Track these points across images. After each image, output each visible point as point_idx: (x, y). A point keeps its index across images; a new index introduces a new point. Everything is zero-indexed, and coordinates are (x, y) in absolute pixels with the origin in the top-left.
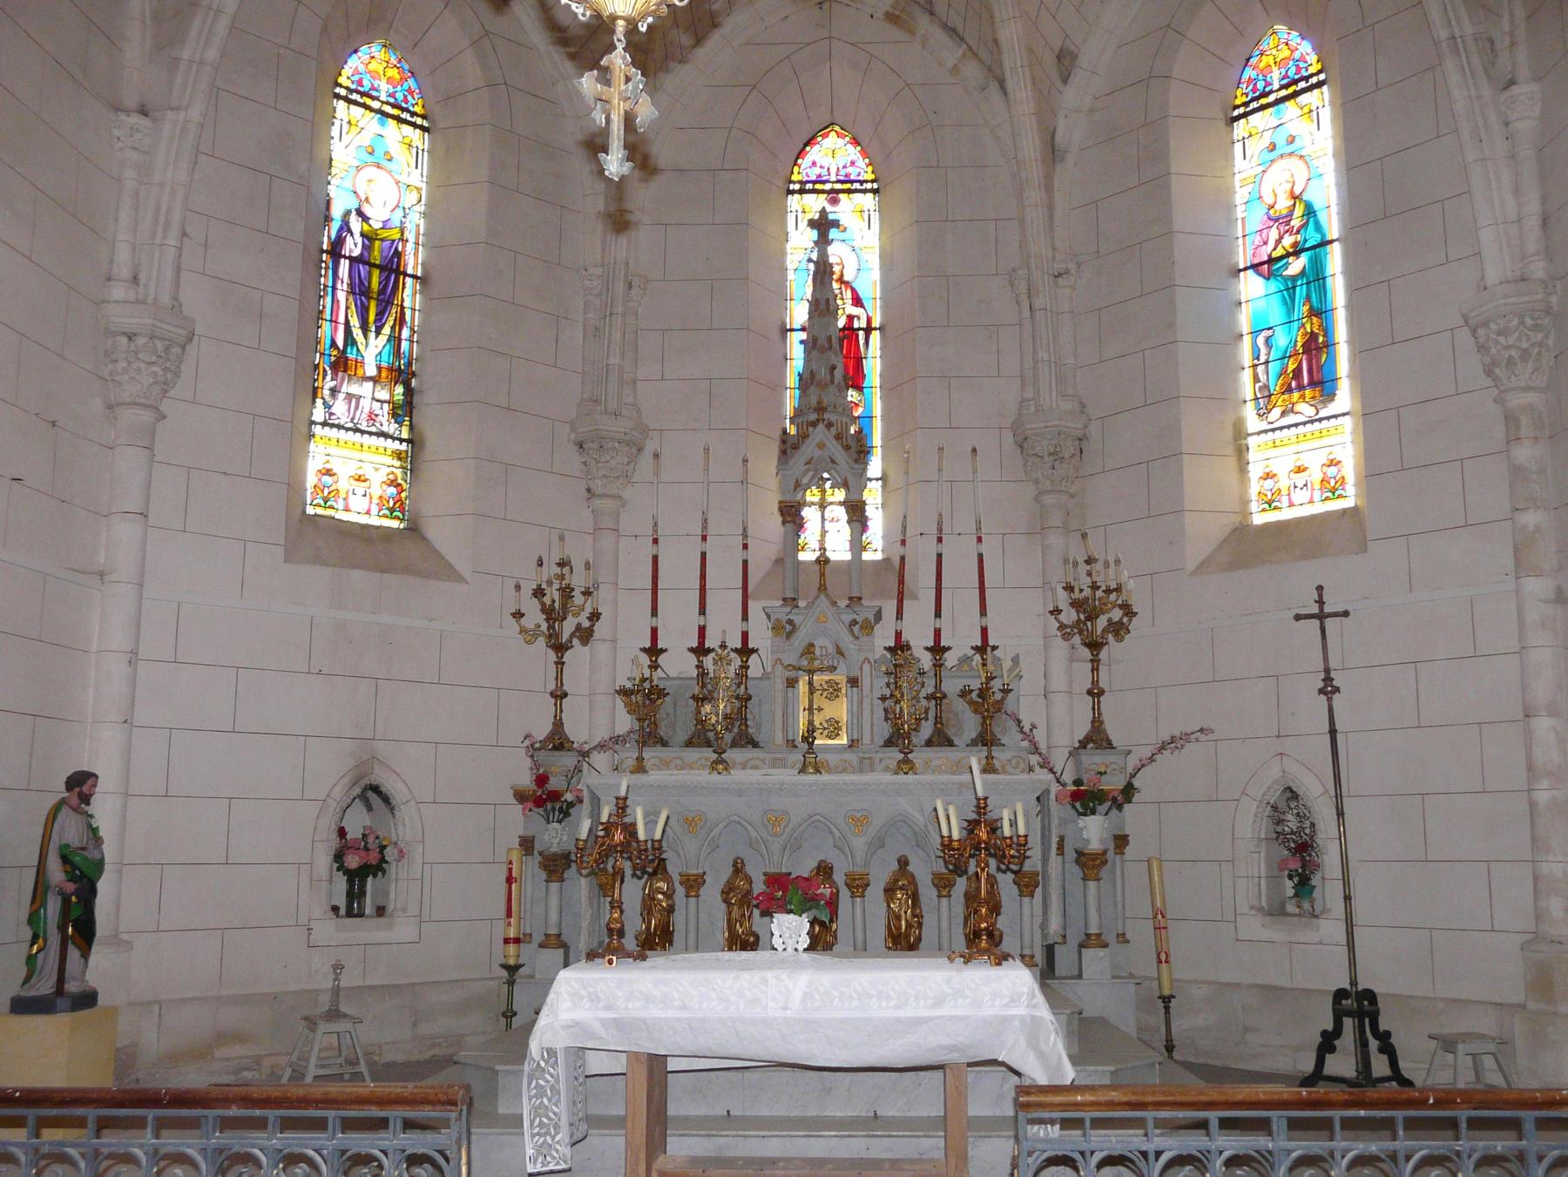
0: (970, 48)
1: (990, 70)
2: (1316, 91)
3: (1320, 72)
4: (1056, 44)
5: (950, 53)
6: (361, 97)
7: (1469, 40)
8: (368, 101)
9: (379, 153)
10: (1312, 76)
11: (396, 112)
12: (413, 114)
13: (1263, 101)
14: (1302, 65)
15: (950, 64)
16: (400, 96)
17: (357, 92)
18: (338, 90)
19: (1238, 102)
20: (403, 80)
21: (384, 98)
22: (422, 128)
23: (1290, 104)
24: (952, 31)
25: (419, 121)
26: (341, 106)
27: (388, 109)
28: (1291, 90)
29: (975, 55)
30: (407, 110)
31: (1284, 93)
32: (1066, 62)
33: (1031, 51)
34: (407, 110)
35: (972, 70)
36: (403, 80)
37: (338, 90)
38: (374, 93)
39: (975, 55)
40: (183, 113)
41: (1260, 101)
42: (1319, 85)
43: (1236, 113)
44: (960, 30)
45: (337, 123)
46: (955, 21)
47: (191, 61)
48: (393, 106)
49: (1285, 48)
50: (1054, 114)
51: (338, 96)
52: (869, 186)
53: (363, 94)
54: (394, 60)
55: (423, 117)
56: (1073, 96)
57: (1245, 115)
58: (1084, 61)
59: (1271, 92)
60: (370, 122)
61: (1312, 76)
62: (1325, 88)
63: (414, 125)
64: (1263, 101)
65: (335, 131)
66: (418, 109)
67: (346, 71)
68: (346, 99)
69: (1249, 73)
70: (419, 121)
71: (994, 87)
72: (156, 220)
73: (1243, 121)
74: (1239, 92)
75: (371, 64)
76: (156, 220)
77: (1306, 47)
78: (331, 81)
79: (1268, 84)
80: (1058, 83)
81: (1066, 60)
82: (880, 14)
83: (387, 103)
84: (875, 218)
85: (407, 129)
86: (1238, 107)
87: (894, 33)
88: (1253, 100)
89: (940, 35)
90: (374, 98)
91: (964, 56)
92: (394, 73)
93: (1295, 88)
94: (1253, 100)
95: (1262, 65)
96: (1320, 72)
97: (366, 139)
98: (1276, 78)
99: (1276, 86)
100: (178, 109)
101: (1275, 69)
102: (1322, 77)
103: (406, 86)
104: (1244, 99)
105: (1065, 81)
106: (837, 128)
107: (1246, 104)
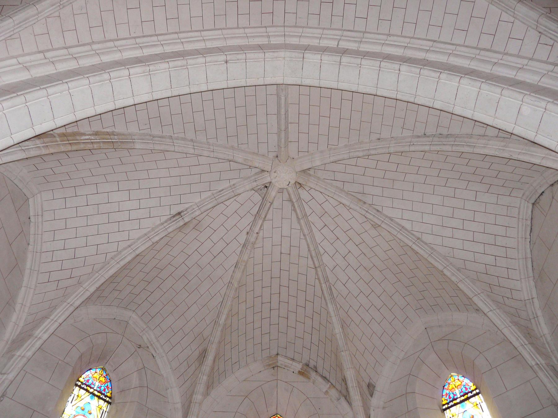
0: (332, 384)
1: (340, 392)
2: (476, 397)
3: (475, 389)
4: (367, 381)
5: (325, 386)
6: (86, 387)
7: (546, 367)
8: (89, 389)
9: (86, 410)
10: (473, 391)
11: (99, 394)
12: (106, 396)
13: (455, 402)
14: (467, 387)
15: (324, 390)
16: (102, 388)
17: (85, 384)
18: (77, 383)
19: (444, 403)
20: (105, 383)
21: (95, 388)
22: (108, 402)
23: (467, 402)
24: (324, 378)
25: (108, 399)
26: (77, 388)
27: (96, 393)
28: (466, 397)
29: (334, 387)
30: (104, 394)
31: (463, 398)
32: (371, 389)
33: (358, 382)
34: (104, 394)
35: (333, 393)
36: (105, 383)
37: (77, 383)
38: (92, 386)
39: (334, 387)
40: (5, 376)
41: (453, 403)
42: (477, 394)
43: (444, 407)
44: (328, 378)
45: (73, 395)
46: (326, 374)
47: (19, 356)
48: (98, 392)
49: (458, 383)
50: (369, 409)
51: (76, 385)
52: (474, 392)
53: (87, 386)
54: (104, 374)
55: (110, 398)
56: (375, 401)
57: (449, 408)
58: (378, 388)
59: (457, 398)
60: (87, 397)
61: (473, 391)
62: (480, 395)
63: (105, 401)
64: (455, 402)
65: (70, 399)
66: (109, 395)
67: (84, 376)
68: (80, 387)
69: (445, 392)
70: (108, 399)
71: (343, 399)
72: (35, 260)
73: (448, 410)
74: (443, 399)
75: (94, 376)
76: (35, 260)
77: (466, 381)
78: (76, 379)
79: (455, 395)
80: (370, 397)
81: (371, 387)
82: (296, 372)
83: (96, 390)
84: (484, 405)
85: (101, 402)
86: (444, 405)
87: (301, 378)
88: (450, 402)
89: (320, 379)
90: (91, 388)
91: (329, 388)
92: (103, 379)
93: (467, 397)
94: (450, 402)
95: (450, 388)
96: (475, 389)
97: (81, 404)
98: (458, 393)
99: (459, 396)
100: (4, 374)
101: (456, 389)
102: (478, 391)
103: (106, 385)
104: (446, 402)
105: (371, 396)
106: (278, 416)
107: (448, 404)
